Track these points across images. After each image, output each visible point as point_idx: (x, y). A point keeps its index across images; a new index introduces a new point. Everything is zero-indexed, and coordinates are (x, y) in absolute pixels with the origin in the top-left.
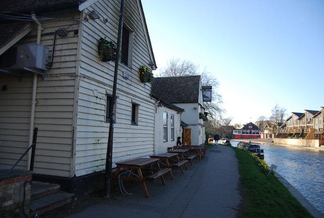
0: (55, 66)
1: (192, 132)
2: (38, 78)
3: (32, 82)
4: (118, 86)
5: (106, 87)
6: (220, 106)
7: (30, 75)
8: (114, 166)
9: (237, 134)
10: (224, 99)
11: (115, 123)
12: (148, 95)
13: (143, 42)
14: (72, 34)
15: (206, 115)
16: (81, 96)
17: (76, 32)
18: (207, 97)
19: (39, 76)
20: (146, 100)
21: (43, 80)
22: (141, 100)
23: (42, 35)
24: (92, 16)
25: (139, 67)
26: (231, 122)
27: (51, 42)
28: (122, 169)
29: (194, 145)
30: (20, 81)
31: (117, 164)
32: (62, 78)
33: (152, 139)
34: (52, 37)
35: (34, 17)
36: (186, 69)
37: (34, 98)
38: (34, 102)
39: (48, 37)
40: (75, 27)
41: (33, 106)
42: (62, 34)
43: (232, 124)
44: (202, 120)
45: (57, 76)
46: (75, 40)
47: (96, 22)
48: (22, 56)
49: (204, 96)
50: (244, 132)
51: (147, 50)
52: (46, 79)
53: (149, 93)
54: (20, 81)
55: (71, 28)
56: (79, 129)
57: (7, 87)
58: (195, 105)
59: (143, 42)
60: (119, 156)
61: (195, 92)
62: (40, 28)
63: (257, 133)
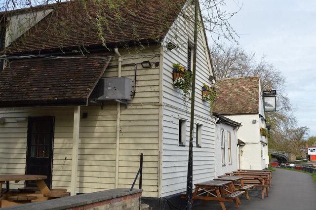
0: (137, 95)
2: (121, 107)
4: (195, 112)
8: (194, 187)
12: (209, 114)
13: (203, 61)
16: (164, 123)
17: (157, 64)
18: (269, 105)
19: (121, 104)
21: (126, 108)
22: (203, 120)
24: (171, 46)
25: (202, 85)
26: (305, 136)
27: (133, 73)
28: (200, 189)
30: (102, 109)
31: (196, 185)
32: (144, 107)
33: (155, 177)
34: (133, 68)
35: (116, 50)
36: (233, 60)
38: (119, 129)
40: (156, 60)
42: (147, 65)
44: (264, 137)
45: (139, 104)
47: (172, 52)
48: (109, 88)
51: (207, 69)
53: (209, 110)
54: (102, 109)
57: (88, 114)
58: (256, 117)
59: (203, 61)
60: (196, 180)
62: (120, 59)
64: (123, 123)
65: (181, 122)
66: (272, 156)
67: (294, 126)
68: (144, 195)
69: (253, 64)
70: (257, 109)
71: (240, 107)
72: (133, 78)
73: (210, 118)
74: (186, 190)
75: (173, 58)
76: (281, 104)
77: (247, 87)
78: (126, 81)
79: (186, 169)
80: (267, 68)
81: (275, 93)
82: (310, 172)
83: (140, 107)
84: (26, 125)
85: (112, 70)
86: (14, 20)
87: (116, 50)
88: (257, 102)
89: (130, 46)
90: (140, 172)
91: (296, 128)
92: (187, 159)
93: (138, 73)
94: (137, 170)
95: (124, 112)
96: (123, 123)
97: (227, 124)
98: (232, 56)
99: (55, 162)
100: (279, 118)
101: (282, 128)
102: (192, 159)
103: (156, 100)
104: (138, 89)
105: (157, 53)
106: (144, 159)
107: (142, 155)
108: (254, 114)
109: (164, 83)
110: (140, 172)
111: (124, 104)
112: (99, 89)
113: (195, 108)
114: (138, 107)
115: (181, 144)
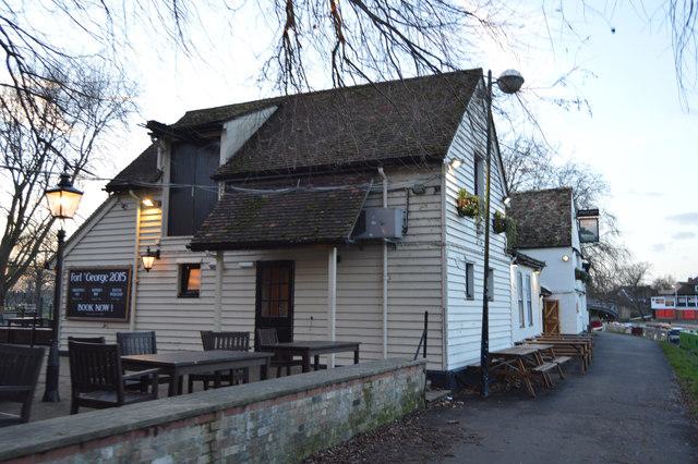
0: (409, 231)
1: (560, 307)
3: (382, 251)
4: (490, 253)
5: (464, 252)
6: (615, 242)
7: (378, 243)
9: (662, 306)
10: (620, 225)
11: (492, 301)
14: (432, 190)
15: (587, 270)
18: (588, 232)
19: (389, 244)
20: (504, 262)
23: (388, 191)
26: (645, 277)
29: (566, 333)
33: (508, 328)
34: (404, 194)
35: (381, 170)
37: (386, 272)
38: (386, 278)
39: (396, 194)
40: (436, 183)
41: (386, 282)
42: (420, 192)
43: (648, 280)
44: (580, 282)
45: (414, 244)
46: (436, 199)
48: (373, 223)
49: (582, 231)
50: (681, 301)
52: (399, 248)
55: (431, 184)
56: (450, 310)
61: (564, 224)
62: (385, 182)
63: (238, 348)
64: (392, 270)
65: (469, 266)
66: (593, 312)
67: (628, 261)
68: (429, 367)
69: (558, 162)
70: (570, 240)
71: (541, 237)
72: (404, 208)
73: (503, 258)
74: (479, 360)
75: (457, 178)
76: (605, 225)
77: (552, 206)
78: (397, 212)
79: (480, 331)
80: (579, 168)
81: (597, 214)
82: (244, 382)
83: (415, 248)
84: (254, 272)
85: (374, 196)
86: (232, 127)
87: (381, 170)
88: (570, 228)
89: (402, 163)
90: (425, 337)
91: (630, 263)
92: (481, 317)
93: (412, 200)
94: (420, 334)
95: (394, 254)
96: (392, 270)
97: (526, 265)
98: (523, 147)
99: (296, 323)
100: (602, 249)
101: (607, 266)
102: (257, 307)
103: (437, 238)
104: (412, 223)
105: (438, 173)
106: (429, 319)
107: (426, 314)
108: (563, 246)
109: (448, 215)
110: (425, 337)
111: (393, 244)
112: (361, 225)
113: (490, 246)
114: (411, 248)
115: (469, 296)
